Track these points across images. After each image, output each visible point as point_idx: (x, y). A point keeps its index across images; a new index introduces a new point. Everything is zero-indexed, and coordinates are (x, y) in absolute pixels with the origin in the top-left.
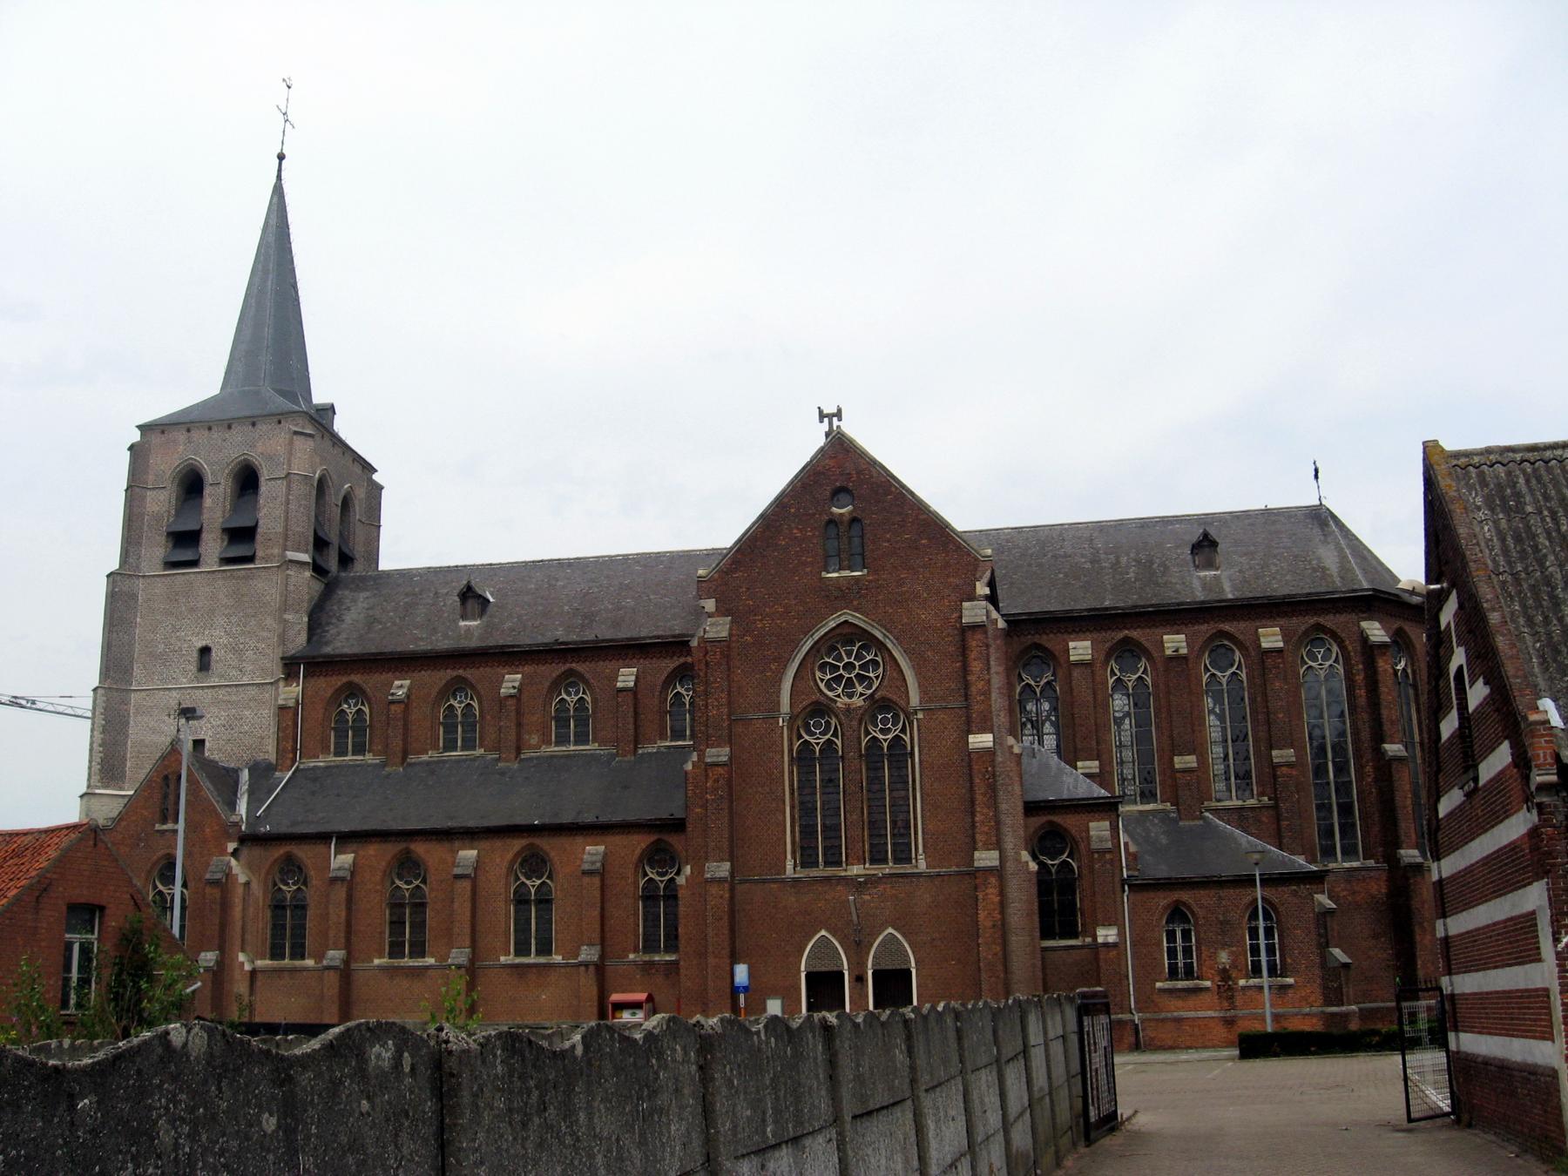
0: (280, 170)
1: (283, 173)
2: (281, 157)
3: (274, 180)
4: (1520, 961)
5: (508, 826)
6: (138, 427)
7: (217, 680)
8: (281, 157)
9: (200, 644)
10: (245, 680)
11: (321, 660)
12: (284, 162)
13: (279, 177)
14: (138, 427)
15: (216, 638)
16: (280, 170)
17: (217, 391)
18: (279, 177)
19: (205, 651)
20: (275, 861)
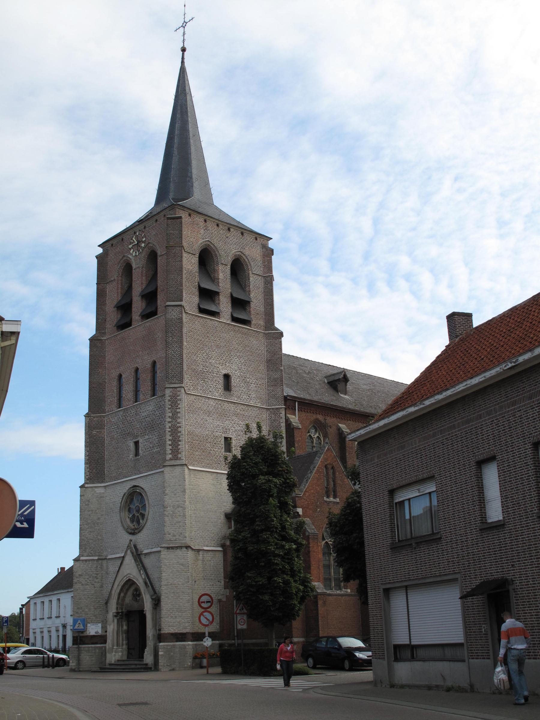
0: (183, 58)
1: (185, 61)
2: (184, 50)
3: (180, 65)
4: (180, 301)
5: (488, 385)
6: (99, 246)
7: (236, 399)
8: (184, 50)
9: (224, 372)
10: (252, 403)
11: (315, 404)
12: (185, 53)
13: (183, 62)
14: (99, 246)
15: (233, 369)
16: (183, 58)
17: (447, 342)
18: (183, 62)
19: (227, 377)
20: (357, 455)
